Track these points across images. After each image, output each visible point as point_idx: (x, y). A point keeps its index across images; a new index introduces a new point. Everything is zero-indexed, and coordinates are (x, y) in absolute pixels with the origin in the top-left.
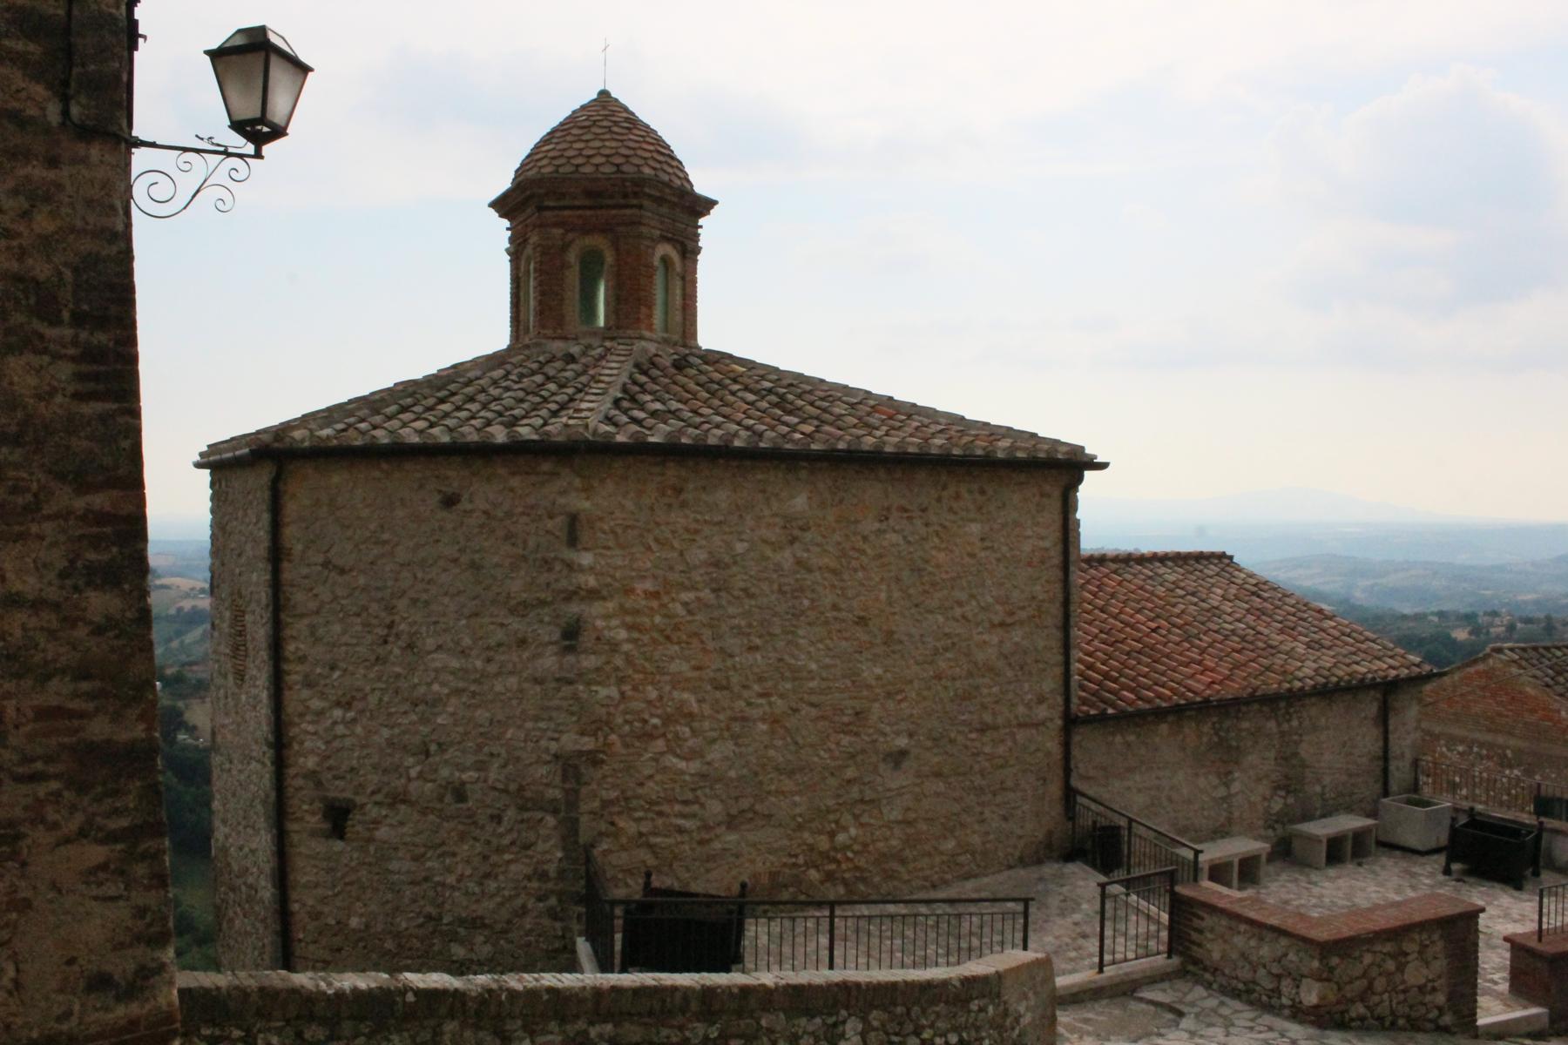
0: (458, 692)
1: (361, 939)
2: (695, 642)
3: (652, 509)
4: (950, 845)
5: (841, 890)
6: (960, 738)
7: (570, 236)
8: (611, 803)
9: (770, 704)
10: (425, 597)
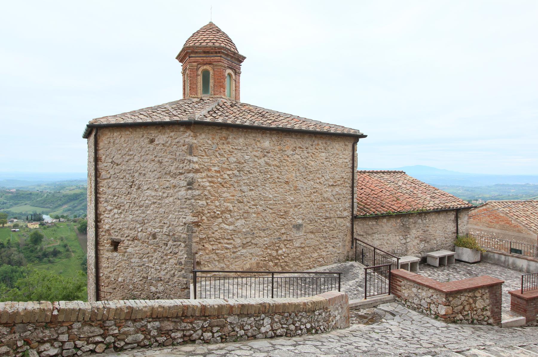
0: (154, 203)
1: (122, 285)
2: (232, 187)
4: (315, 255)
5: (280, 269)
6: (319, 221)
7: (199, 66)
8: (203, 239)
10: (143, 172)
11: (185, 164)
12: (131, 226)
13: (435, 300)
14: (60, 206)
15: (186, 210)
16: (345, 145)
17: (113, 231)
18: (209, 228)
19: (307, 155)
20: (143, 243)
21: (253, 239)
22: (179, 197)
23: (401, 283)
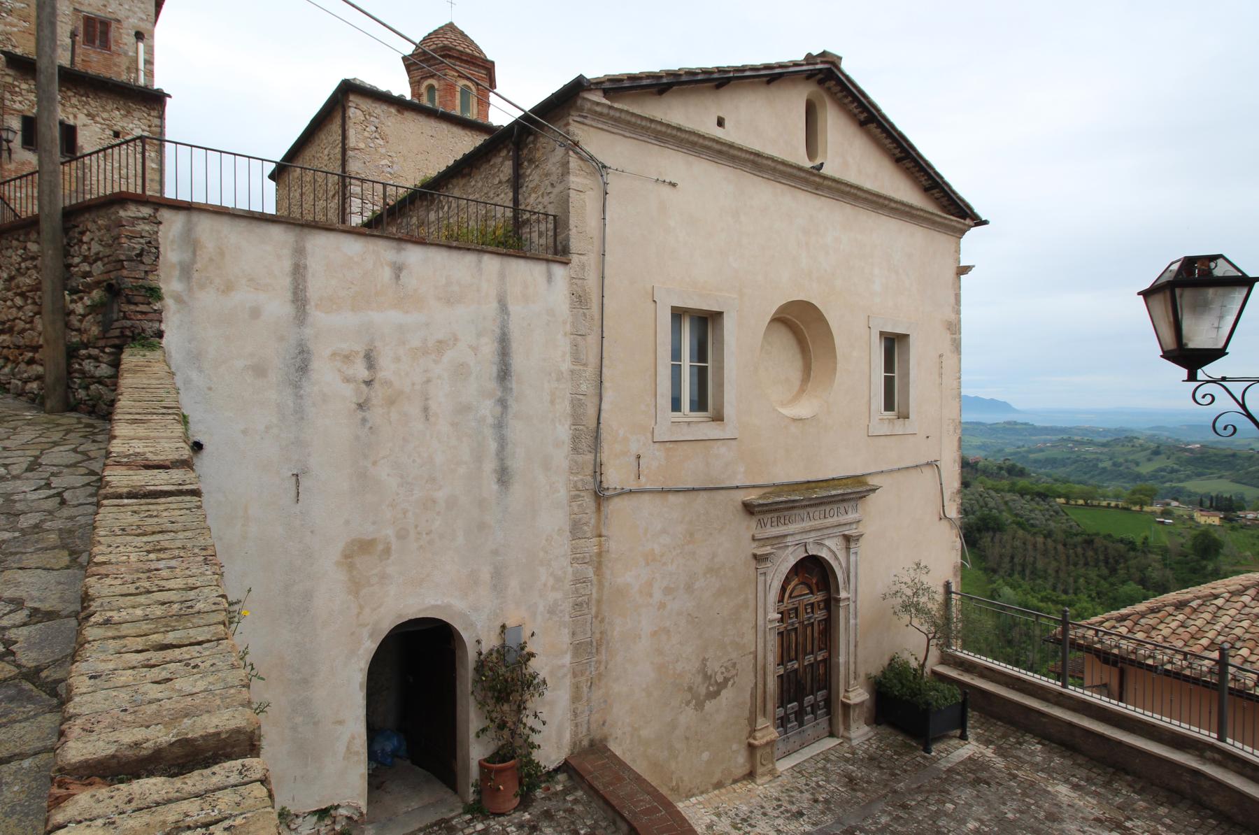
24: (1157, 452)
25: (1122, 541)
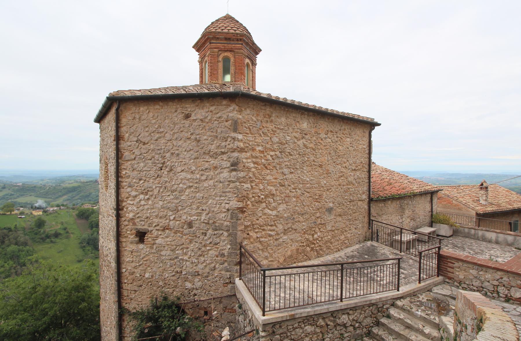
0: (190, 187)
2: (274, 169)
3: (262, 122)
4: (342, 237)
7: (220, 52)
9: (296, 191)
10: (177, 152)
11: (228, 143)
12: (161, 214)
13: (505, 283)
14: (60, 196)
15: (230, 195)
16: (364, 132)
17: (138, 220)
18: (254, 214)
19: (336, 139)
20: (175, 233)
21: (293, 224)
22: (221, 180)
23: (454, 265)
24: (4, 188)
25: (5, 228)
